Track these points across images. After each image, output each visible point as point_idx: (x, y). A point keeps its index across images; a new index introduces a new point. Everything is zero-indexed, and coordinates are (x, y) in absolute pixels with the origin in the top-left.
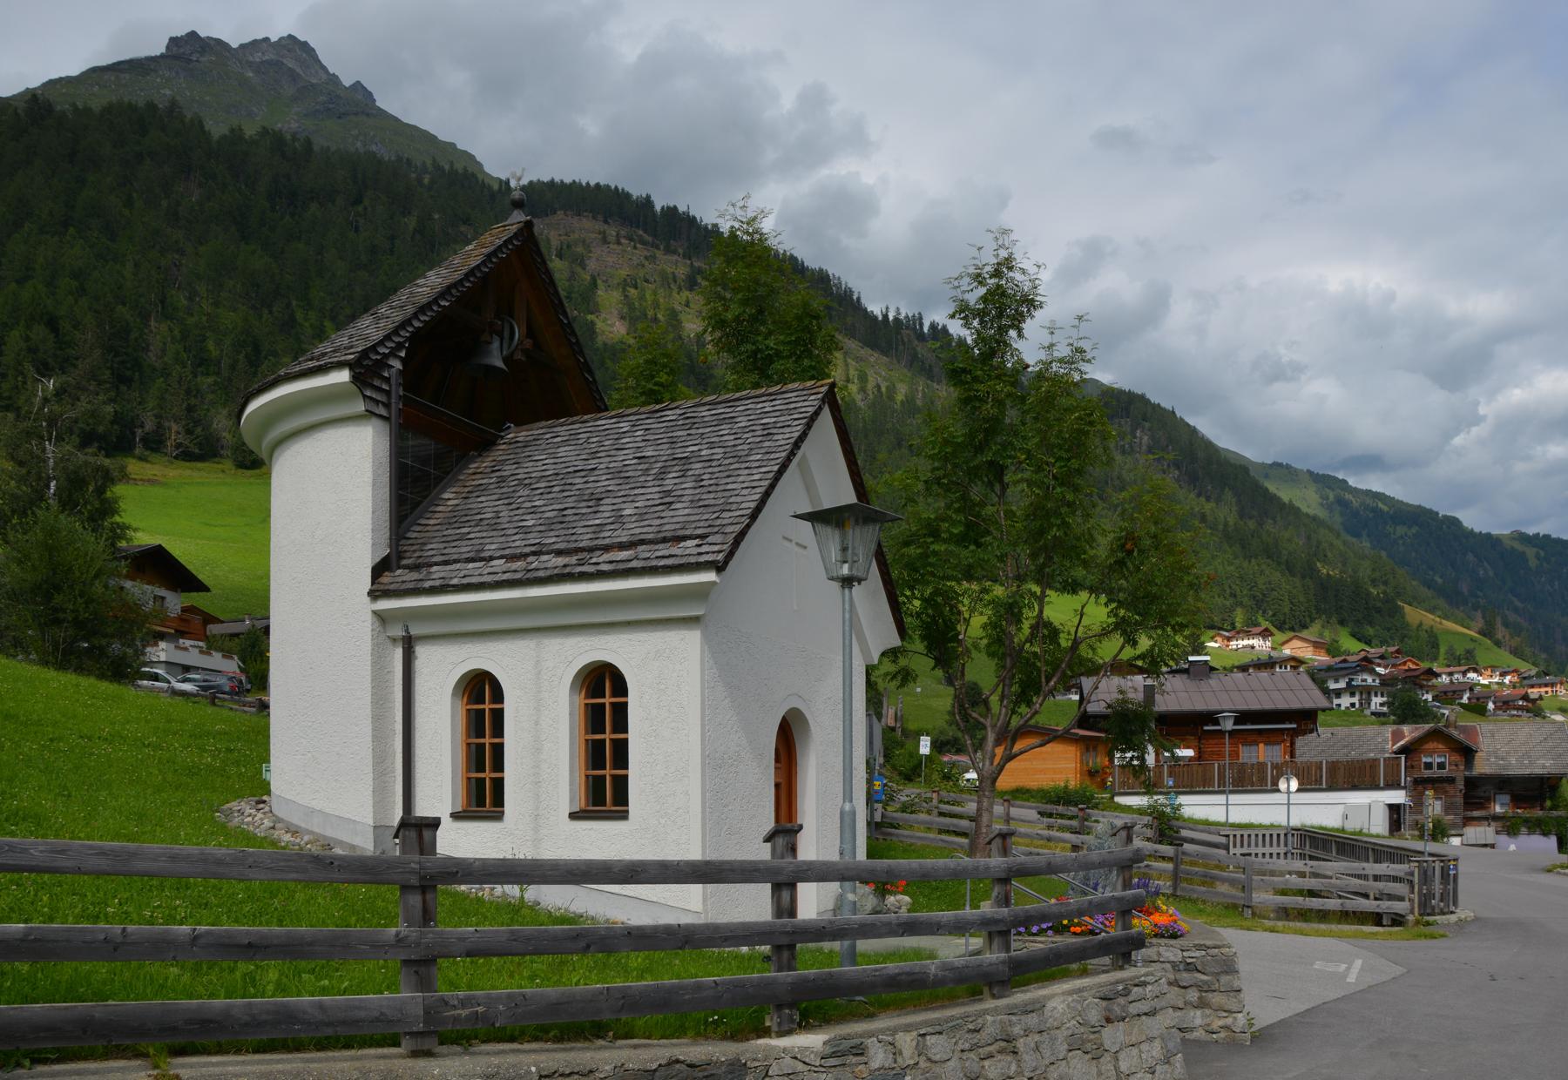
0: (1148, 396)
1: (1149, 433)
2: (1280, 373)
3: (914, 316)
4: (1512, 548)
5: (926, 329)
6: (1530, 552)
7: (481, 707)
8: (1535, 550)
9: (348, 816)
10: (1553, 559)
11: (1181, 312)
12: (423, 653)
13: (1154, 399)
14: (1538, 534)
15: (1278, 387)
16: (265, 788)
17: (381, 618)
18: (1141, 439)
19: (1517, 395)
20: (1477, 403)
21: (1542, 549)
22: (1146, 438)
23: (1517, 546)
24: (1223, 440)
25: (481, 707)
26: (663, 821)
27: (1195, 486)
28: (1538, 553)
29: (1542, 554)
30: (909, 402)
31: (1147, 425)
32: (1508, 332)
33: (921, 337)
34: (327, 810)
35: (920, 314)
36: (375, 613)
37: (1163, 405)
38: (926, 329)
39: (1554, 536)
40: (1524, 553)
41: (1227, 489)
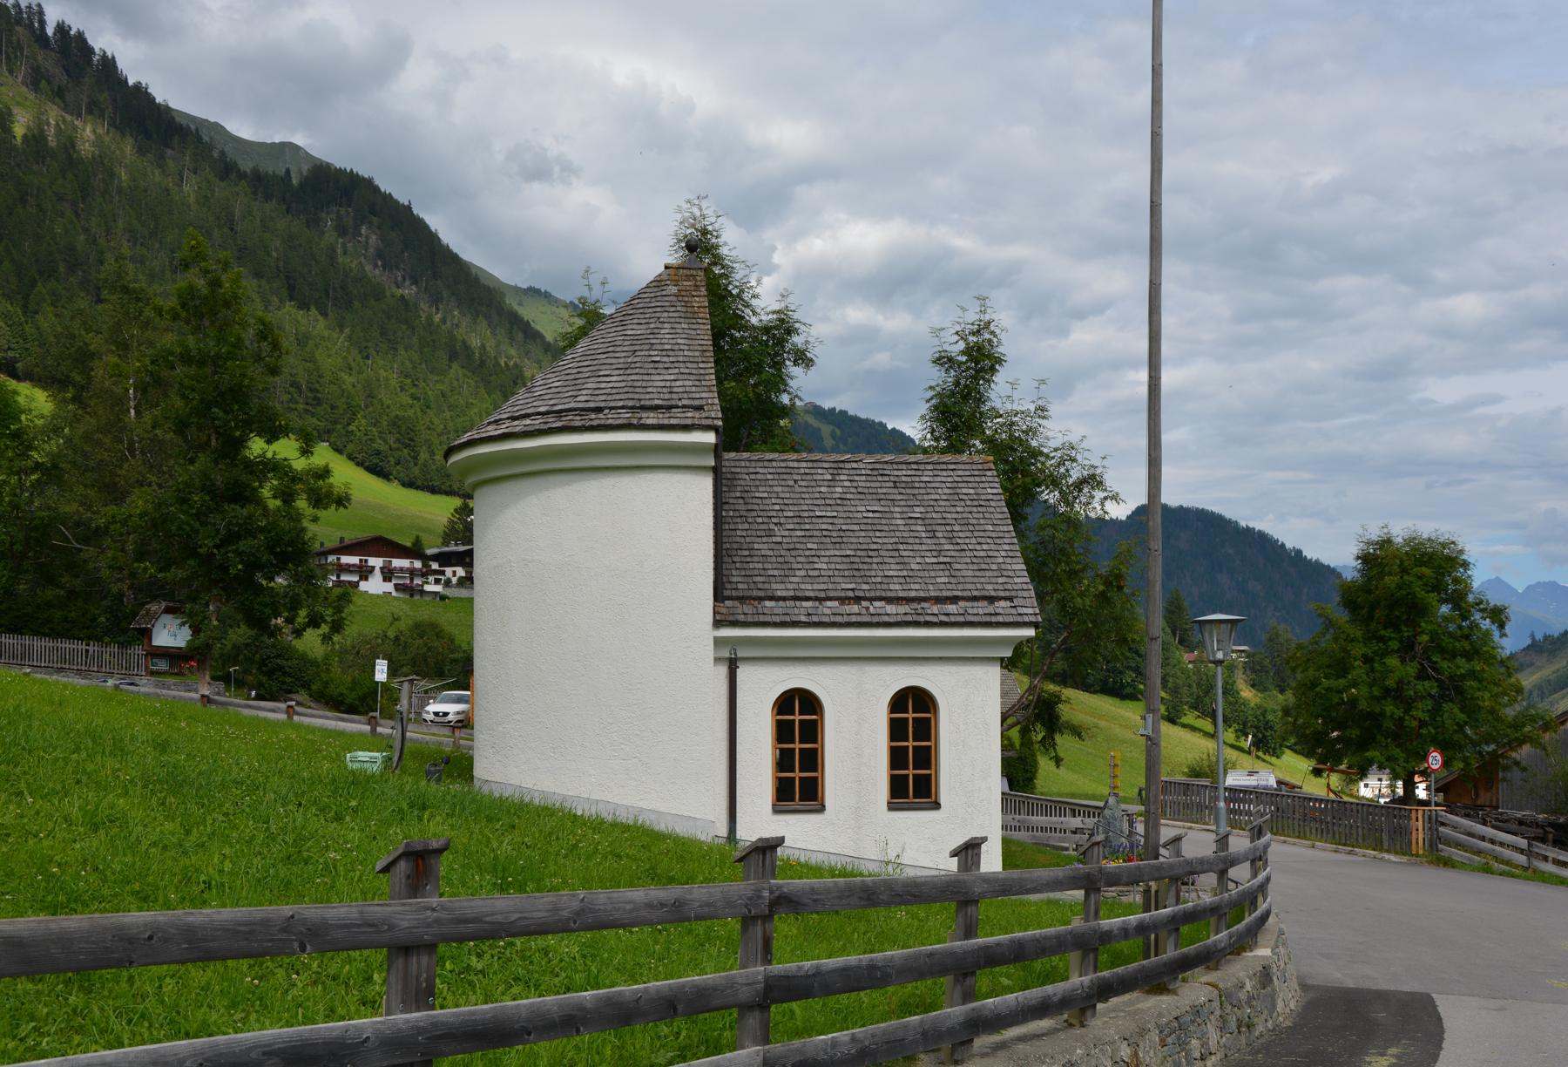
0: (377, 182)
1: (377, 231)
2: (539, 171)
3: (29, 7)
4: (806, 422)
5: (50, 31)
6: (826, 430)
7: (791, 717)
8: (831, 427)
9: (686, 814)
10: (850, 440)
11: (416, 77)
12: (743, 672)
13: (384, 187)
14: (835, 408)
15: (537, 187)
16: (472, 777)
17: (718, 642)
18: (367, 238)
19: (816, 246)
20: (774, 249)
21: (839, 428)
22: (374, 237)
23: (811, 420)
24: (470, 254)
25: (791, 717)
26: (969, 810)
27: (437, 309)
28: (833, 431)
29: (838, 432)
30: (36, 139)
31: (375, 220)
32: (810, 173)
33: (42, 38)
34: (662, 810)
35: (39, 5)
36: (715, 638)
37: (395, 196)
38: (50, 31)
39: (851, 413)
40: (819, 429)
41: (481, 317)
